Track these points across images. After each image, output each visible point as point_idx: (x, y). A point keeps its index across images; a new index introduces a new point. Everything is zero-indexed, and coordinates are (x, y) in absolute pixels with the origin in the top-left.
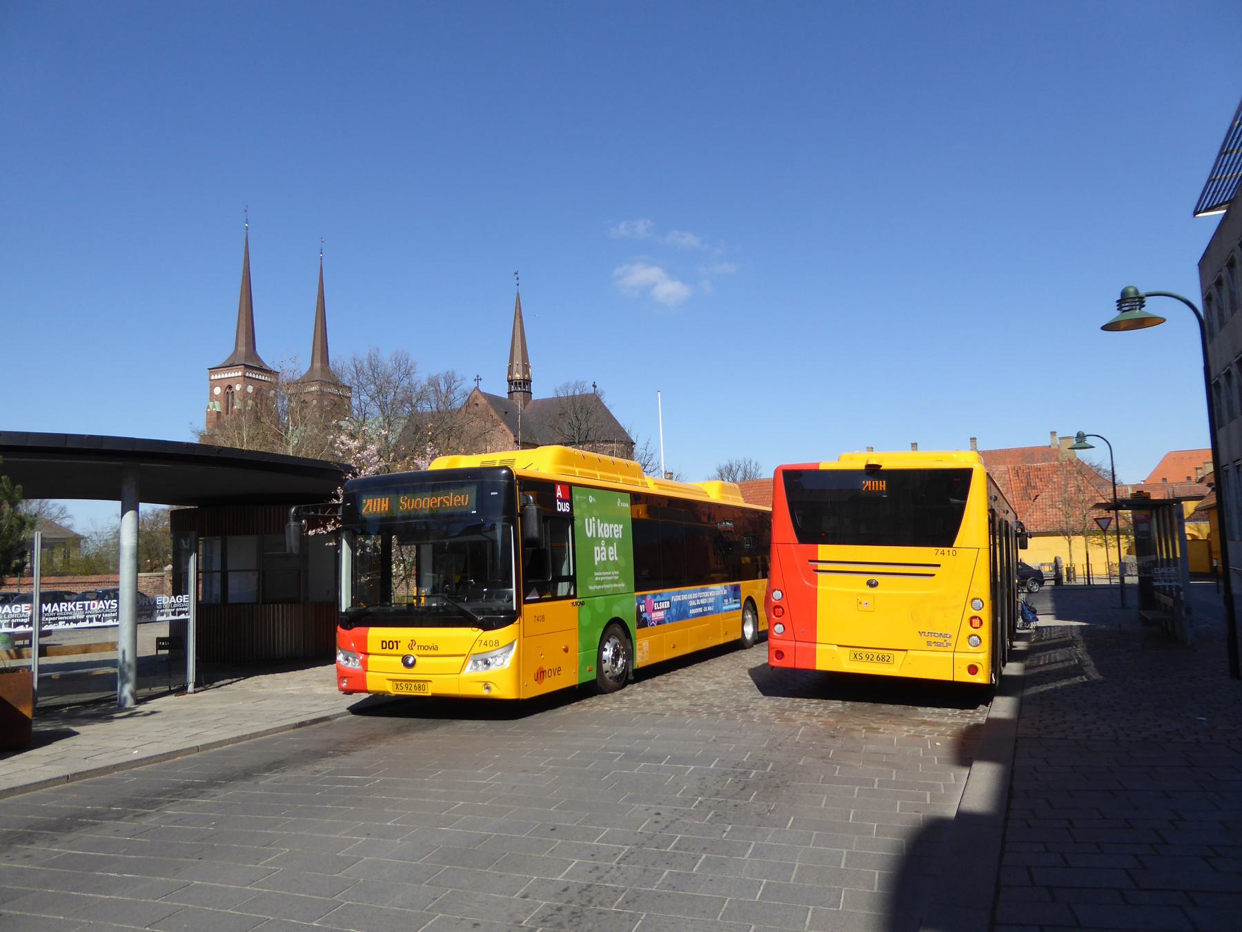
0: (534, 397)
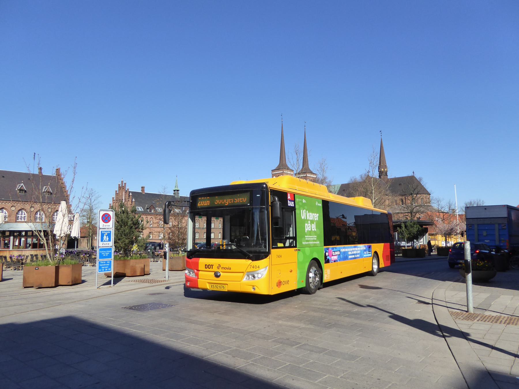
0: (389, 177)
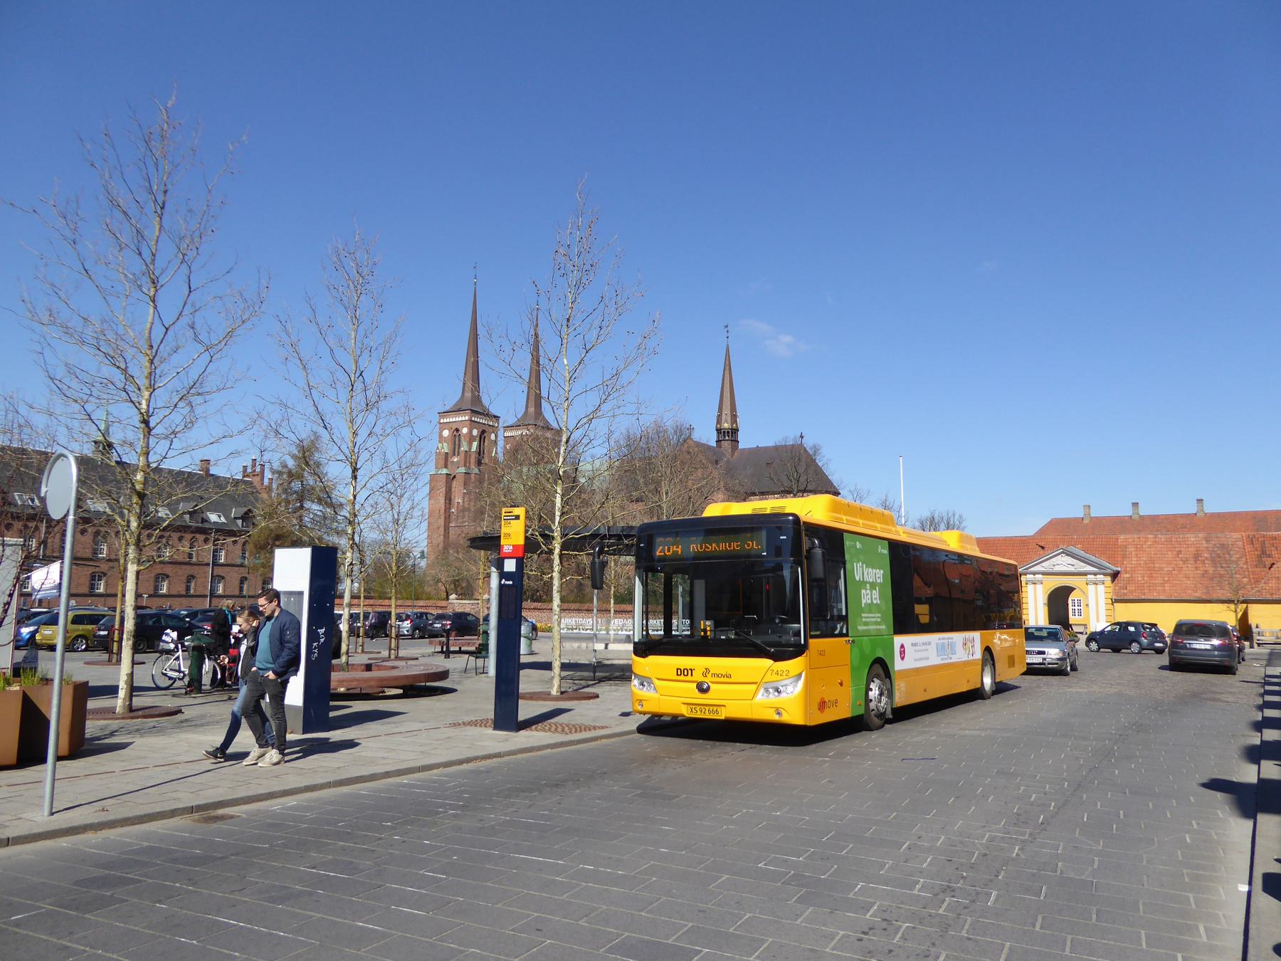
0: (741, 446)
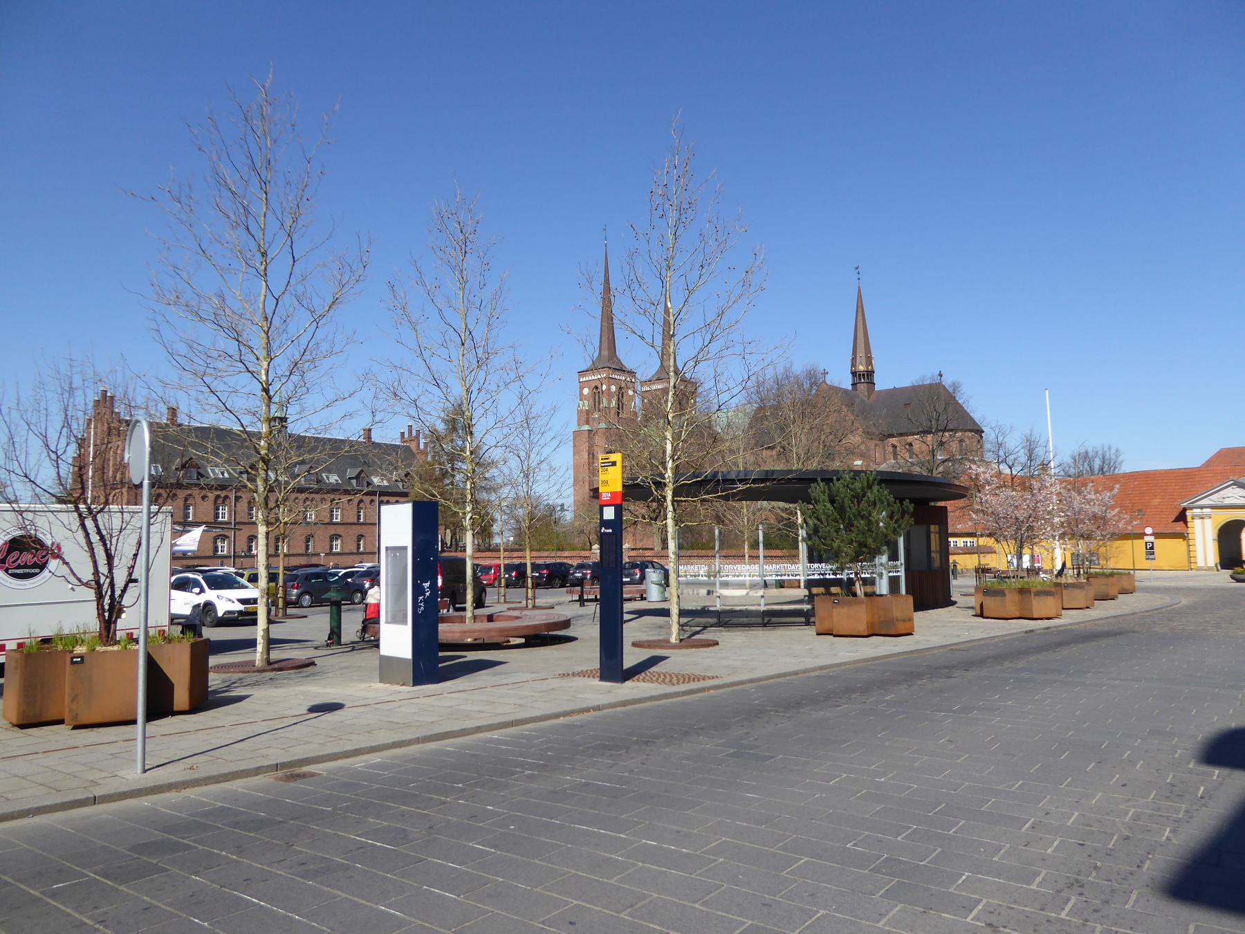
0: (877, 388)
